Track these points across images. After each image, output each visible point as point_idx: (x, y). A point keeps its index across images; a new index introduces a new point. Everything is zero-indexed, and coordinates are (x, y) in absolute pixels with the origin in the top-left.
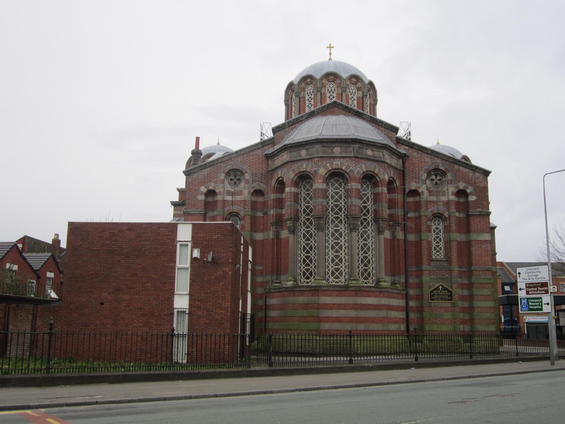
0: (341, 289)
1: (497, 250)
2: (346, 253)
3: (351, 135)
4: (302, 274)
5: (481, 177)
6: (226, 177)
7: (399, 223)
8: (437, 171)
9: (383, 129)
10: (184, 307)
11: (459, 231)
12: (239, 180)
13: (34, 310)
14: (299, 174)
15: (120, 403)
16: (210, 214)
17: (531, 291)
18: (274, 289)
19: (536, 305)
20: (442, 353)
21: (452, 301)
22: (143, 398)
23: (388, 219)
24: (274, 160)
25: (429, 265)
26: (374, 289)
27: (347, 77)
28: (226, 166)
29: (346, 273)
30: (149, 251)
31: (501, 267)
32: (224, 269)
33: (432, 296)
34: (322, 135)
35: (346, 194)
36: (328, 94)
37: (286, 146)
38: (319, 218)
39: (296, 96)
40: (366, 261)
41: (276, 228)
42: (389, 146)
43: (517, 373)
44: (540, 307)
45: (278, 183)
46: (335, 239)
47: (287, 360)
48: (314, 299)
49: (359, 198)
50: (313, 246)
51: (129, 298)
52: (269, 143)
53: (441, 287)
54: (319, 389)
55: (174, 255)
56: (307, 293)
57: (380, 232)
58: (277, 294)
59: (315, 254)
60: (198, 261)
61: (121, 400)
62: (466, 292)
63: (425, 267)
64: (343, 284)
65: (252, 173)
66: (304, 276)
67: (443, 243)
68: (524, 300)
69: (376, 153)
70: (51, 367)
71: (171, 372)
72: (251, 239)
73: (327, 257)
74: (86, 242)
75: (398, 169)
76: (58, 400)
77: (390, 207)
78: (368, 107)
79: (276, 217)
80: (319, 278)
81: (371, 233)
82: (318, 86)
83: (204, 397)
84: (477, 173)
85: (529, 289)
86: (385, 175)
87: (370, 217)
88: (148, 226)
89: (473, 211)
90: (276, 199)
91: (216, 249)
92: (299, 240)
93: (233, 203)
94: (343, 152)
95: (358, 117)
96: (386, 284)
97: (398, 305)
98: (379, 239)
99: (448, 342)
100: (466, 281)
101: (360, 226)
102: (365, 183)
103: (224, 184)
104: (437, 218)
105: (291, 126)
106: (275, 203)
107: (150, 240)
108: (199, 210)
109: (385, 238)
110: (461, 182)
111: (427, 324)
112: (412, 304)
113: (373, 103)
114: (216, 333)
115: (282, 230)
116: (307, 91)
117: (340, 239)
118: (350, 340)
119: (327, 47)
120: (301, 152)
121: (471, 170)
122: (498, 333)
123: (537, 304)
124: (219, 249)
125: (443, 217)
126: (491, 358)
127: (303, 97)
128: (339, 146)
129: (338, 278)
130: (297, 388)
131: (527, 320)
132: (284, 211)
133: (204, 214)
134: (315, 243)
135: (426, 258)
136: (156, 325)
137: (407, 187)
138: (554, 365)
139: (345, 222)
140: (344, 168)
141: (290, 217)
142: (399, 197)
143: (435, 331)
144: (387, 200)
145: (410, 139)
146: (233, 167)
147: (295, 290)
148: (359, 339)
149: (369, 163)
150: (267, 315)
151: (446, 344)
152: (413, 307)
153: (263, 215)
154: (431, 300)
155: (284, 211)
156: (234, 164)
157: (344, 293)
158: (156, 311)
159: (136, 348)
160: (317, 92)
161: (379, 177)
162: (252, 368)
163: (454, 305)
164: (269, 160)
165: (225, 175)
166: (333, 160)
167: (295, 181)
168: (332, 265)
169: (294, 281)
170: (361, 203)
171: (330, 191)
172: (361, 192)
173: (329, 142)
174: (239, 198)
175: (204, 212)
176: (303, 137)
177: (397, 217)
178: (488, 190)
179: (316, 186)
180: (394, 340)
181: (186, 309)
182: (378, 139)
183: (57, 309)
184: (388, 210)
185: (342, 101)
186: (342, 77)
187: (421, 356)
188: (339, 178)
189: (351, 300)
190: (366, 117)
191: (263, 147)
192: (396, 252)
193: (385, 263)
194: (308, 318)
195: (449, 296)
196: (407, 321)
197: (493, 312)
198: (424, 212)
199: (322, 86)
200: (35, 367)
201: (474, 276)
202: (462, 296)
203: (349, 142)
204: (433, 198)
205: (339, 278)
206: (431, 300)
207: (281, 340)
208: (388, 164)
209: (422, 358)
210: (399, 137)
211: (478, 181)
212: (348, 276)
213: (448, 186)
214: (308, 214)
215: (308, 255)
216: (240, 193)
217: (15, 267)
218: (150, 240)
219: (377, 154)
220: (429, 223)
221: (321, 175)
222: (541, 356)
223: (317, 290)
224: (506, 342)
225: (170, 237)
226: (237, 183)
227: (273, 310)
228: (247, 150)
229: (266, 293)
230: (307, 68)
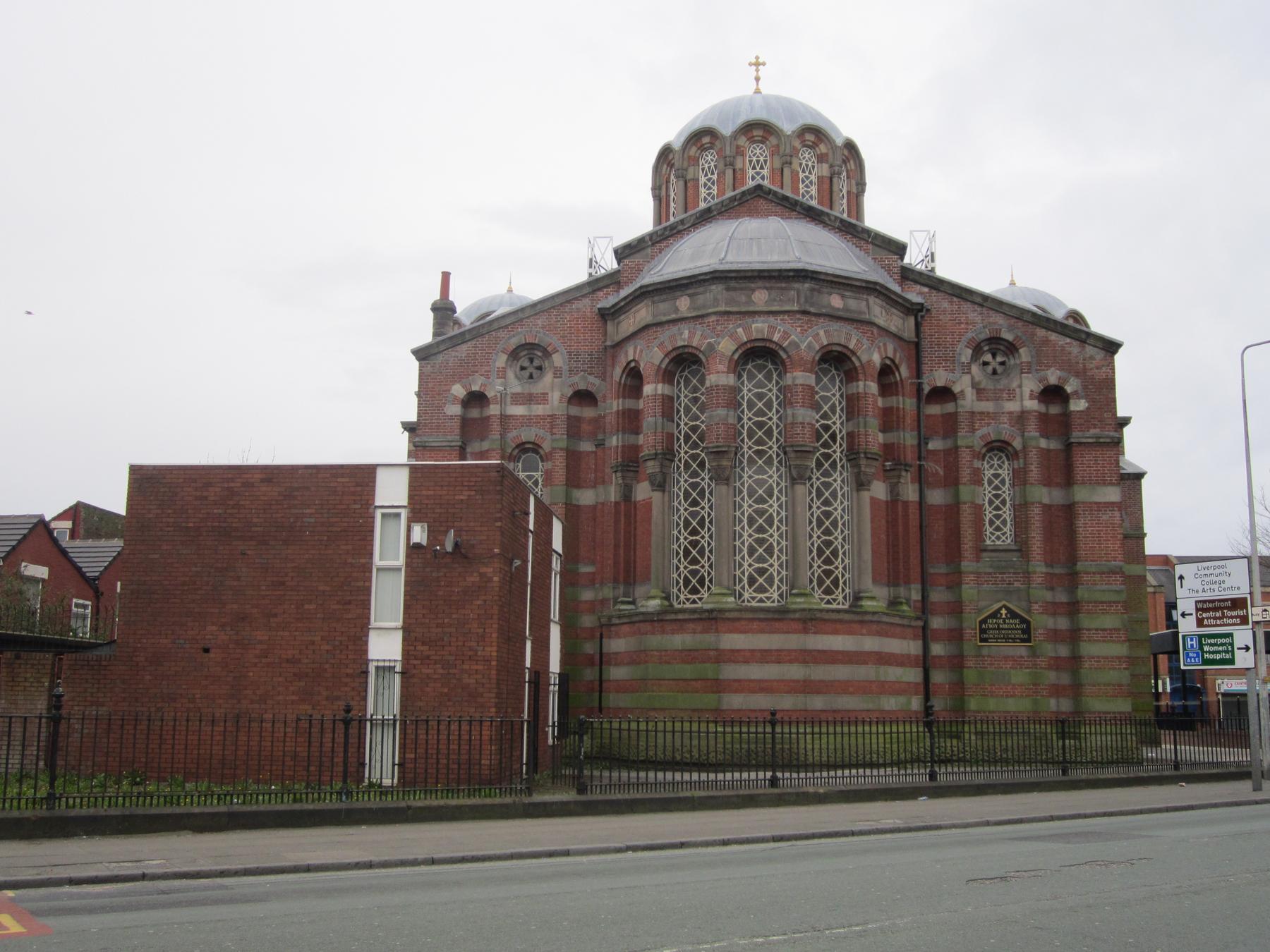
0: (770, 616)
1: (1148, 527)
2: (782, 533)
3: (792, 262)
4: (681, 581)
5: (1099, 355)
6: (509, 363)
8: (995, 343)
9: (870, 246)
10: (388, 658)
11: (1047, 482)
13: (53, 664)
14: (674, 354)
15: (201, 878)
16: (475, 447)
17: (1207, 618)
18: (619, 617)
19: (1219, 652)
20: (1007, 762)
22: (256, 865)
23: (880, 456)
24: (618, 323)
25: (978, 559)
26: (847, 617)
27: (793, 132)
29: (781, 580)
30: (311, 529)
31: (1164, 568)
32: (483, 570)
33: (983, 631)
34: (727, 263)
35: (782, 397)
36: (750, 170)
37: (645, 290)
38: (719, 454)
39: (677, 177)
40: (828, 552)
41: (623, 478)
43: (1167, 810)
44: (1228, 656)
45: (628, 375)
46: (756, 502)
47: (638, 778)
48: (707, 640)
49: (811, 407)
50: (706, 517)
51: (267, 638)
52: (608, 282)
53: (1004, 611)
54: (682, 845)
55: (369, 538)
56: (691, 625)
57: (861, 484)
58: (626, 628)
59: (711, 537)
60: (424, 551)
61: (202, 871)
62: (1063, 623)
63: (967, 565)
64: (776, 604)
65: (570, 353)
66: (685, 588)
67: (1010, 510)
68: (1192, 640)
69: (853, 304)
70: (58, 795)
71: (343, 806)
72: (566, 504)
73: (738, 543)
74: (170, 511)
75: (905, 341)
76: (56, 870)
77: (885, 429)
78: (845, 201)
79: (623, 452)
80: (719, 591)
81: (842, 488)
82: (728, 153)
83: (403, 863)
84: (1091, 347)
85: (1204, 615)
86: (873, 354)
87: (839, 451)
88: (310, 471)
89: (1080, 434)
91: (463, 524)
92: (676, 504)
93: (528, 421)
94: (775, 300)
95: (812, 221)
96: (875, 604)
97: (905, 652)
99: (1021, 738)
100: (1062, 597)
101: (815, 470)
102: (826, 372)
103: (505, 378)
104: (996, 452)
105: (657, 242)
107: (315, 505)
108: (449, 438)
109: (872, 498)
110: (1053, 369)
111: (972, 695)
112: (937, 649)
113: (854, 190)
114: (449, 717)
115: (638, 482)
116: (703, 165)
117: (768, 502)
118: (773, 733)
119: (750, 64)
120: (677, 304)
122: (1150, 716)
123: (1221, 648)
124: (472, 524)
125: (1010, 448)
126: (1122, 772)
130: (629, 844)
131: (1224, 688)
132: (641, 440)
133: (461, 447)
134: (712, 510)
135: (970, 544)
136: (327, 698)
138: (1260, 789)
139: (780, 462)
140: (776, 338)
141: (654, 451)
142: (906, 403)
143: (990, 712)
144: (876, 411)
145: (933, 270)
146: (525, 339)
147: (665, 619)
148: (809, 730)
149: (836, 326)
150: (604, 677)
151: (1015, 742)
152: (941, 657)
153: (594, 449)
154: (980, 642)
155: (641, 440)
157: (777, 624)
158: (327, 666)
159: (284, 751)
160: (726, 166)
161: (858, 358)
162: (537, 798)
163: (1034, 653)
165: (508, 359)
168: (750, 561)
169: (662, 598)
170: (817, 417)
171: (745, 391)
172: (817, 393)
173: (741, 278)
174: (539, 410)
175: (459, 444)
176: (683, 268)
177: (902, 449)
178: (1114, 385)
179: (713, 380)
180: (891, 733)
181: (395, 661)
182: (856, 269)
183: (104, 663)
184: (881, 435)
185: (782, 188)
186: (782, 131)
187: (943, 770)
188: (767, 361)
189: (793, 641)
190: (830, 220)
191: (594, 291)
192: (901, 529)
193: (873, 556)
194: (694, 683)
195: (1024, 631)
196: (927, 689)
197: (1124, 669)
198: (964, 438)
199: (737, 153)
200: (35, 794)
201: (1083, 584)
202: (1055, 631)
203: (789, 277)
204: (988, 406)
205: (766, 591)
206: (982, 640)
207: (634, 734)
208: (879, 327)
209: (947, 775)
210: (908, 266)
211: (1092, 366)
212: (787, 586)
213: (1021, 377)
214: (695, 446)
215: (694, 538)
216: (543, 398)
217: (41, 572)
218: (315, 505)
219: (855, 304)
220: (977, 464)
221: (723, 355)
222: (1233, 770)
223: (715, 619)
224: (1182, 738)
225: (358, 498)
226: (534, 376)
227: (617, 665)
228: (558, 301)
229: (602, 626)
230: (700, 114)
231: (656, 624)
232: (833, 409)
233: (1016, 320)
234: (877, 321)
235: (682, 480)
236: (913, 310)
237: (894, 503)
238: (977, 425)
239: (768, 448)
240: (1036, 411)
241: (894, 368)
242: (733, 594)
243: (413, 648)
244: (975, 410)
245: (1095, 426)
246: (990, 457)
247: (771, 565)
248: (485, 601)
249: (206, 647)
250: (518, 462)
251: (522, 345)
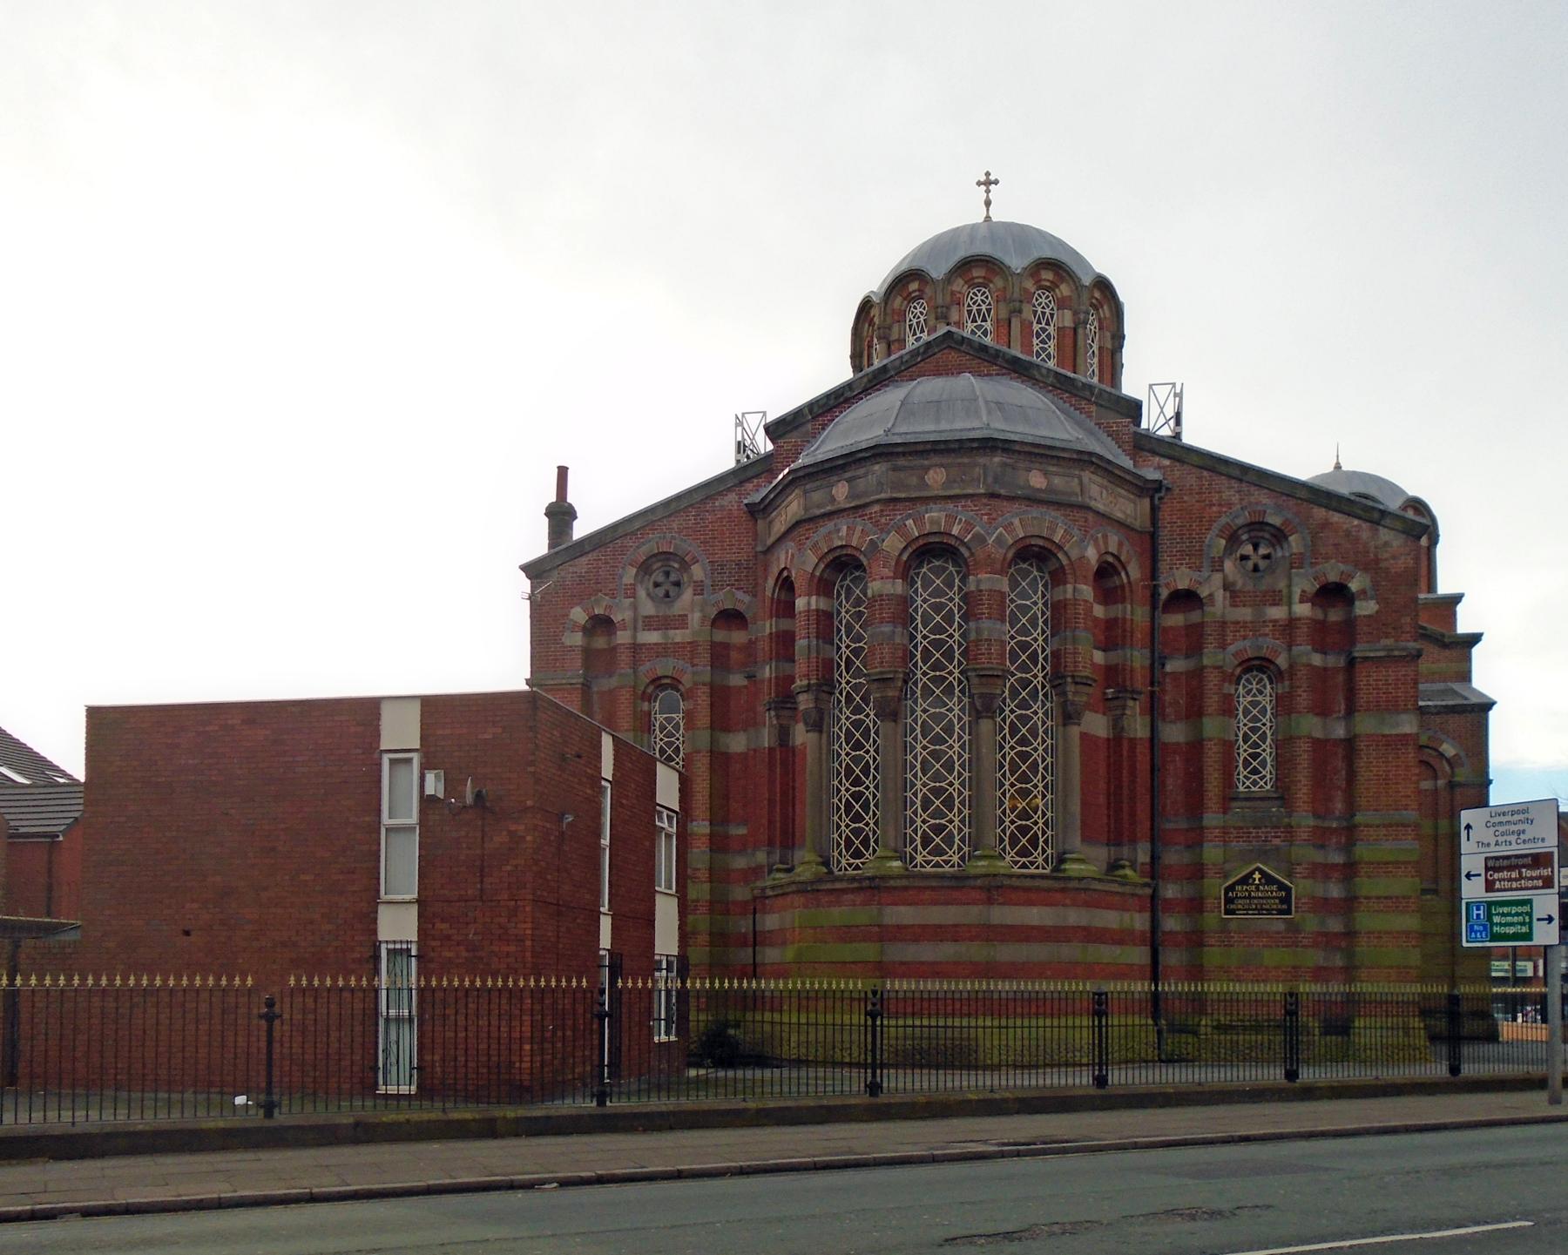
0: (946, 883)
7: (1133, 692)
9: (1093, 408)
10: (399, 939)
12: (677, 584)
14: (830, 557)
17: (1500, 880)
21: (1290, 914)
24: (770, 522)
28: (638, 547)
32: (513, 828)
33: (1228, 901)
41: (778, 717)
42: (1100, 457)
44: (1524, 929)
53: (1257, 876)
56: (850, 896)
57: (1069, 716)
63: (1212, 819)
68: (1478, 909)
78: (1096, 360)
79: (777, 685)
81: (1044, 723)
85: (1496, 876)
86: (1086, 549)
90: (778, 635)
93: (662, 650)
94: (955, 481)
98: (1065, 740)
100: (1337, 858)
103: (634, 598)
106: (774, 645)
109: (1084, 736)
110: (1333, 561)
112: (1171, 923)
113: (1109, 345)
116: (910, 320)
119: (979, 184)
121: (1366, 520)
123: (1515, 919)
125: (1272, 667)
127: (898, 340)
128: (942, 465)
129: (942, 853)
133: (583, 684)
137: (1162, 580)
140: (955, 531)
142: (1137, 614)
149: (1035, 512)
154: (1225, 914)
156: (660, 538)
161: (1066, 554)
164: (759, 521)
165: (637, 572)
166: (924, 508)
167: (820, 579)
174: (678, 636)
179: (875, 589)
182: (1066, 436)
188: (946, 562)
189: (972, 914)
190: (1042, 375)
191: (741, 483)
199: (952, 302)
201: (1362, 840)
203: (972, 449)
204: (1245, 613)
208: (1097, 513)
209: (900, 1083)
211: (1386, 555)
219: (1062, 482)
220: (1229, 688)
223: (878, 888)
226: (671, 594)
227: (772, 945)
231: (810, 896)
232: (1033, 621)
233: (1285, 498)
234: (1093, 504)
235: (843, 717)
236: (1148, 489)
237: (1116, 741)
238: (1229, 639)
239: (948, 673)
240: (1307, 618)
241: (1120, 568)
242: (902, 858)
243: (430, 926)
244: (1229, 618)
245: (1387, 636)
246: (1248, 680)
247: (951, 821)
248: (516, 866)
249: (186, 929)
250: (655, 701)
251: (655, 555)
